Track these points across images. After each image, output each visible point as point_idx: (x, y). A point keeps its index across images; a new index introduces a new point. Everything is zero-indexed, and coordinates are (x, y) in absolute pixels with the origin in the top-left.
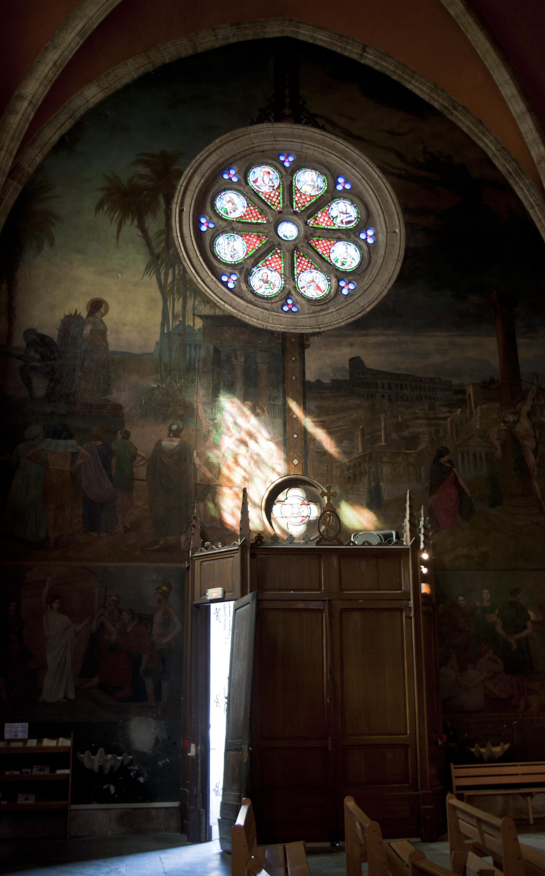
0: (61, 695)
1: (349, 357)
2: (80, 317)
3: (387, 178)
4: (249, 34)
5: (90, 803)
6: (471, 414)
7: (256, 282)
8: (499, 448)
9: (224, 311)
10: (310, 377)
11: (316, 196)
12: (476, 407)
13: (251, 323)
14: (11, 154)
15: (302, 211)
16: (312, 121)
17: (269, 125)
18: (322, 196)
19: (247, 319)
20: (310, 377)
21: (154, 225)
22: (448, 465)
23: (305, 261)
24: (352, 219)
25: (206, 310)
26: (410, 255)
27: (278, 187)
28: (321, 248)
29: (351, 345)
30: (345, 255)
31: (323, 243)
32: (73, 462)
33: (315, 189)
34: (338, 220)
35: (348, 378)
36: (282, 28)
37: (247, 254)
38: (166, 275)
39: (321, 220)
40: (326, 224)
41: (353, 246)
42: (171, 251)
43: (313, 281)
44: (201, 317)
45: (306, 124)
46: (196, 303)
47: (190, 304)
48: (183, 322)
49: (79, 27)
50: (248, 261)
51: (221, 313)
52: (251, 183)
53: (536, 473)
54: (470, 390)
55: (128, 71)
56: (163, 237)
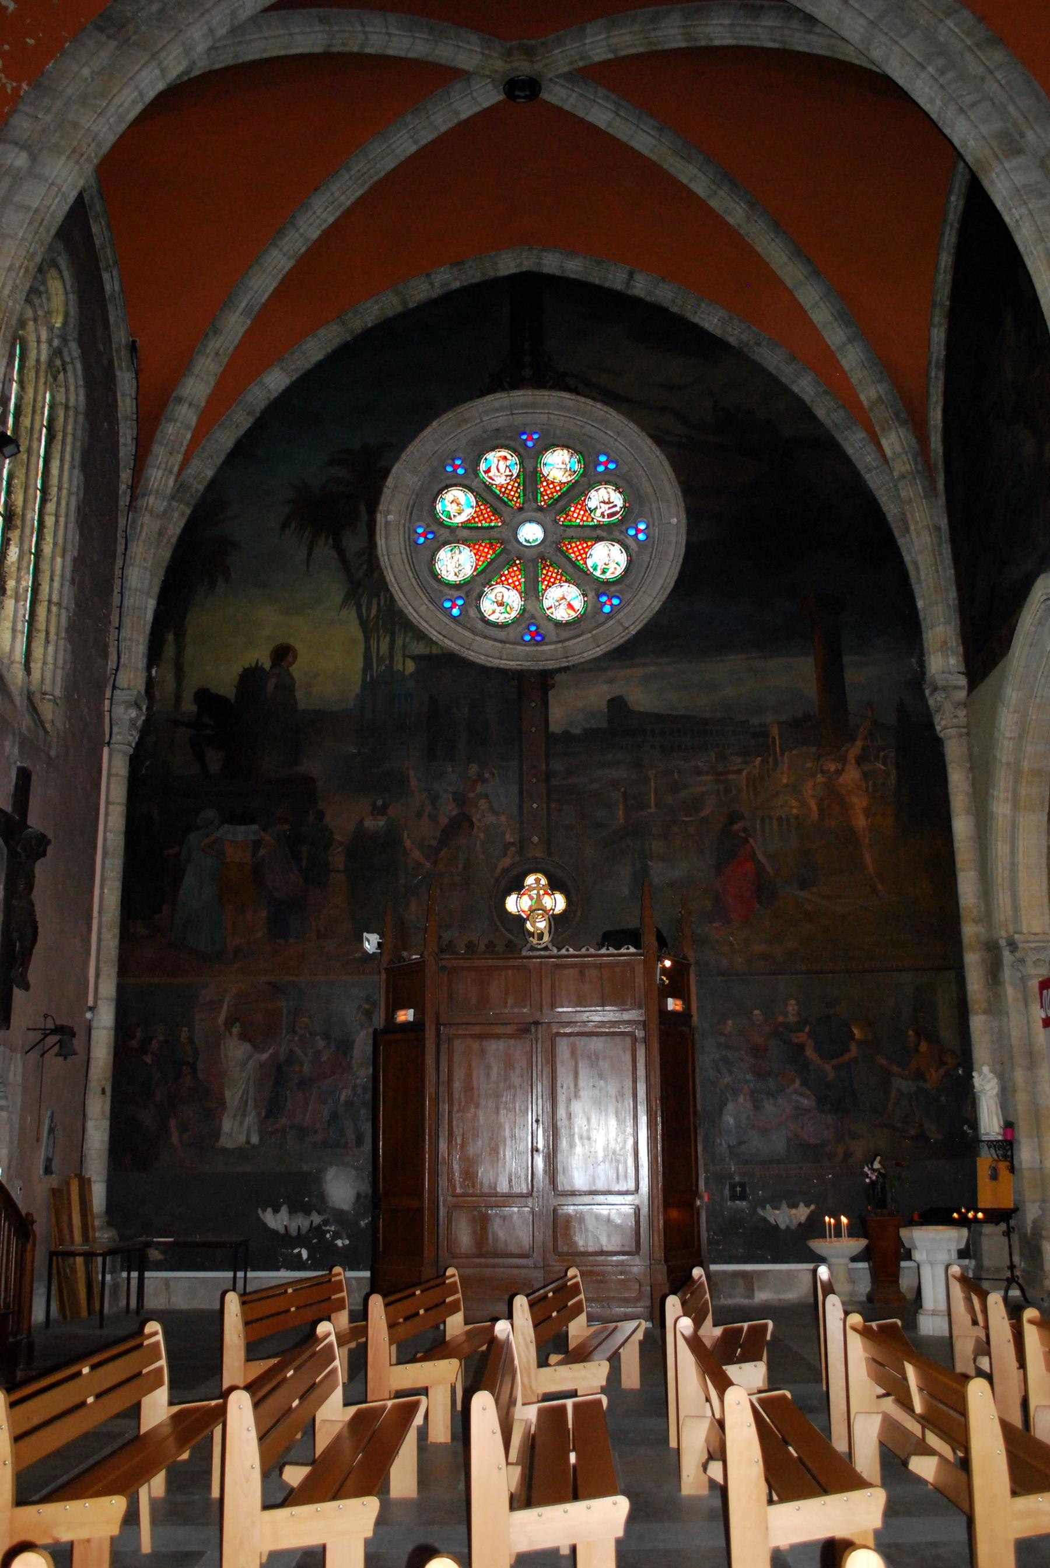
0: (242, 1139)
1: (609, 697)
2: (262, 669)
3: (663, 450)
4: (472, 274)
5: (278, 1269)
6: (775, 761)
7: (487, 606)
8: (815, 808)
9: (442, 648)
10: (555, 728)
11: (568, 483)
12: (782, 755)
13: (478, 661)
14: (171, 472)
15: (549, 506)
16: (561, 383)
17: (504, 395)
18: (577, 482)
19: (472, 656)
20: (555, 728)
21: (353, 544)
22: (742, 834)
23: (552, 572)
24: (617, 509)
25: (419, 649)
26: (693, 554)
27: (518, 476)
28: (574, 552)
29: (611, 681)
30: (607, 559)
31: (577, 546)
32: (255, 853)
33: (567, 474)
34: (598, 513)
35: (605, 725)
36: (519, 261)
37: (476, 569)
38: (369, 609)
39: (575, 515)
40: (582, 520)
41: (617, 547)
42: (375, 575)
43: (563, 598)
44: (413, 658)
45: (553, 388)
46: (408, 640)
47: (399, 643)
48: (390, 667)
49: (243, 304)
50: (478, 578)
51: (440, 652)
52: (482, 474)
53: (867, 841)
54: (775, 731)
55: (314, 350)
56: (365, 557)
